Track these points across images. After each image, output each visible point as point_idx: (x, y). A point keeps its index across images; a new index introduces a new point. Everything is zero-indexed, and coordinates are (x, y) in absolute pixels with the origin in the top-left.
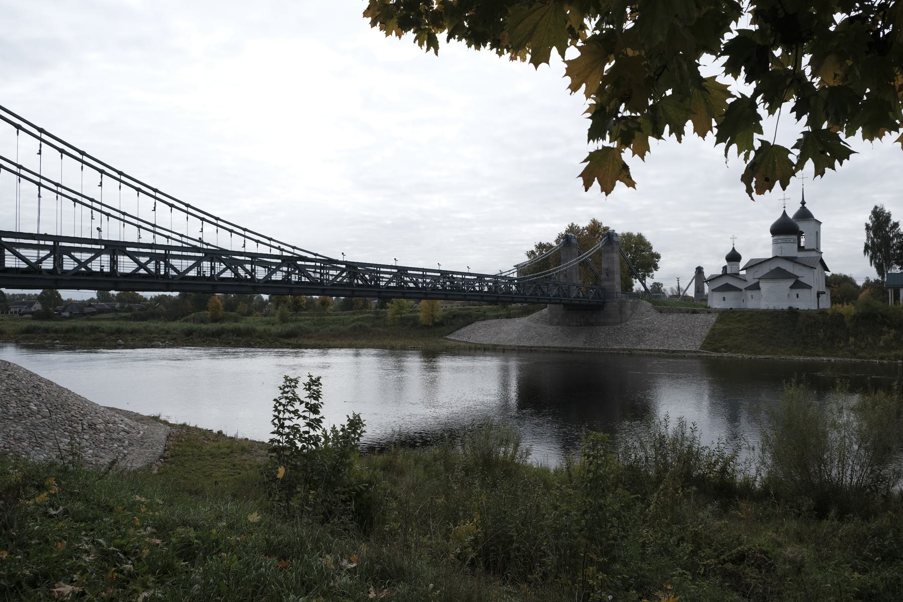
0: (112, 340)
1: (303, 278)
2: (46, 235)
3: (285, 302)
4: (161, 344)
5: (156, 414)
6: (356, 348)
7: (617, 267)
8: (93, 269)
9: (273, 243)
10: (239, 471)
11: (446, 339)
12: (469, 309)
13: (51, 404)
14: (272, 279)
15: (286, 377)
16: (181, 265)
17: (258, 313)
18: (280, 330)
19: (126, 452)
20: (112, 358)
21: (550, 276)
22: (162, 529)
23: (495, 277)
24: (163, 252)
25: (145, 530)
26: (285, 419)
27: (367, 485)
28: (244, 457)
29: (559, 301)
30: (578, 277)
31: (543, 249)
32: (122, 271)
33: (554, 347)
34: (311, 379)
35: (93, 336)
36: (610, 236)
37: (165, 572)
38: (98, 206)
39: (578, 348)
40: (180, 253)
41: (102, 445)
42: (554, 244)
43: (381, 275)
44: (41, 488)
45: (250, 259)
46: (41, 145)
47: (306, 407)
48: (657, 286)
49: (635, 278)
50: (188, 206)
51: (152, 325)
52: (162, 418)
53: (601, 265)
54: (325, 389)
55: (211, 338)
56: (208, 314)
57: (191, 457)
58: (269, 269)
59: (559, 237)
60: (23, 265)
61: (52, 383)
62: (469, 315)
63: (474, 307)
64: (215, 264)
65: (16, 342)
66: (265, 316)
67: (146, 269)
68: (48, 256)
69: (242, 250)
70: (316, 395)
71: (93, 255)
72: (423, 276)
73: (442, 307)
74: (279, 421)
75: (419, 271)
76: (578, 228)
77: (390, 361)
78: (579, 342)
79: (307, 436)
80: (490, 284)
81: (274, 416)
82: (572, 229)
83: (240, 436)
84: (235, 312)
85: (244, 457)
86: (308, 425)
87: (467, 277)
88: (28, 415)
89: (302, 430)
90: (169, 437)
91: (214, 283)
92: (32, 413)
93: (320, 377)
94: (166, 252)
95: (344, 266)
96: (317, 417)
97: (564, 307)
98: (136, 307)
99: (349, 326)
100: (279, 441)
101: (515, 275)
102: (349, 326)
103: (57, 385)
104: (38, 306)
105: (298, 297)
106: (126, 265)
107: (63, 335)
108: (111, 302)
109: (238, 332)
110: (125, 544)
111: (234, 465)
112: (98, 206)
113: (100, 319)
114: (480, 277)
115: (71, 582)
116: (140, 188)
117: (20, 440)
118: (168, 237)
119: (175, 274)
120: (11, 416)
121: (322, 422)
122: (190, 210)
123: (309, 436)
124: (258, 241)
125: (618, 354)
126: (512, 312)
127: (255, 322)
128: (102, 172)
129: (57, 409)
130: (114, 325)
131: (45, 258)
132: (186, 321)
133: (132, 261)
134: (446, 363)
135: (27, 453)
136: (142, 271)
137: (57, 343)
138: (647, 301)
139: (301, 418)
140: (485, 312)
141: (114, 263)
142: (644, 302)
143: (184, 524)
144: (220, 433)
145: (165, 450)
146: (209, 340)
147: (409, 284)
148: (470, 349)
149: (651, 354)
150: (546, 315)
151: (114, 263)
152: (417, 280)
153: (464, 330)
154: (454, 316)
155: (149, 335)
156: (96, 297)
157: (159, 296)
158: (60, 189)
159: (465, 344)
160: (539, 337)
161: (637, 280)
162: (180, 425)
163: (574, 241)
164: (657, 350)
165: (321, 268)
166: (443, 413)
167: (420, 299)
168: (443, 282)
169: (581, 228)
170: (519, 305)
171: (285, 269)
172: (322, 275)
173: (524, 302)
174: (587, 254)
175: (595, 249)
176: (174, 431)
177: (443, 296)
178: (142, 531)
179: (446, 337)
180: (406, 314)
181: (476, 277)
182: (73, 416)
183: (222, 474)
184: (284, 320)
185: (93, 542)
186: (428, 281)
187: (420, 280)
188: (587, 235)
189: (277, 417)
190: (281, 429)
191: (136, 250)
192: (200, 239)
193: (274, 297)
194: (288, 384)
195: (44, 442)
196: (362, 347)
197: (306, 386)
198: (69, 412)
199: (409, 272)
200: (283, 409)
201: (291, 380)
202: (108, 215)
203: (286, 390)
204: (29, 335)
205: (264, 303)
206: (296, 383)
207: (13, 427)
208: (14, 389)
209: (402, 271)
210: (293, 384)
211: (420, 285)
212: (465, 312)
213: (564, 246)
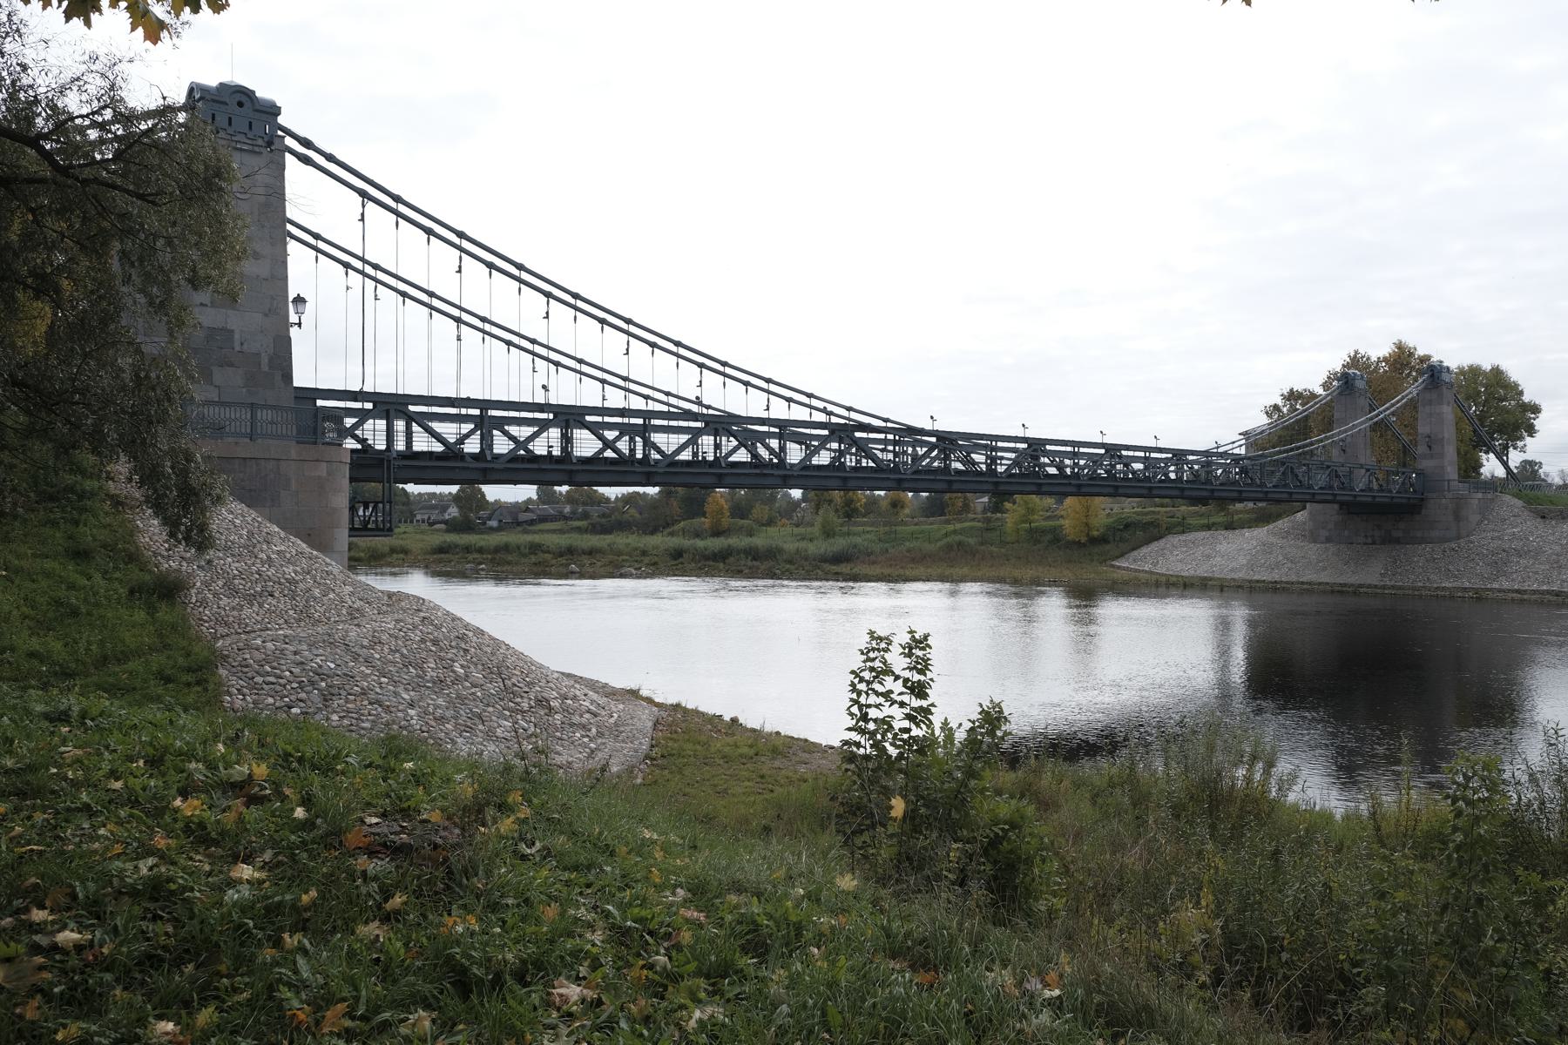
0: (562, 565)
1: (864, 461)
2: (468, 399)
3: (830, 501)
4: (634, 572)
5: (634, 686)
6: (952, 582)
7: (1449, 433)
8: (536, 452)
9: (815, 402)
10: (770, 786)
11: (1113, 566)
12: (1154, 512)
13: (483, 665)
14: (813, 462)
15: (871, 633)
16: (667, 442)
17: (784, 520)
18: (823, 550)
19: (592, 745)
20: (560, 594)
21: (1311, 451)
22: (699, 892)
23: (1207, 453)
24: (640, 421)
25: (674, 894)
26: (869, 706)
27: (1007, 827)
28: (777, 764)
29: (1330, 498)
30: (1368, 452)
31: (1296, 400)
32: (579, 454)
33: (1320, 584)
34: (913, 636)
35: (533, 559)
36: (1434, 374)
37: (717, 974)
38: (543, 351)
39: (1369, 586)
40: (665, 423)
41: (558, 734)
42: (1320, 391)
43: (999, 454)
44: (504, 808)
45: (777, 430)
46: (460, 257)
47: (905, 686)
48: (1530, 467)
49: (1487, 452)
50: (678, 344)
51: (621, 540)
52: (644, 693)
53: (1415, 428)
54: (937, 655)
55: (711, 563)
56: (706, 522)
57: (692, 759)
58: (807, 447)
59: (1329, 378)
60: (438, 448)
61: (482, 633)
62: (1153, 524)
63: (1164, 509)
64: (721, 440)
65: (426, 567)
66: (797, 526)
67: (615, 450)
68: (472, 432)
69: (765, 415)
70: (922, 666)
71: (536, 429)
72: (1074, 455)
73: (1105, 510)
74: (860, 709)
75: (1067, 445)
76: (1368, 359)
77: (1012, 607)
78: (1371, 573)
79: (906, 736)
80: (1196, 467)
81: (852, 700)
82: (1355, 361)
83: (768, 728)
84: (747, 519)
85: (777, 764)
86: (909, 717)
87: (1153, 455)
88: (451, 681)
89: (897, 725)
90: (656, 723)
91: (720, 471)
92: (457, 680)
93: (929, 635)
94: (645, 421)
95: (933, 439)
96: (924, 703)
97: (1341, 509)
98: (594, 511)
99: (939, 544)
100: (858, 745)
101: (1243, 451)
102: (939, 544)
103: (490, 636)
104: (453, 512)
105: (851, 493)
106: (585, 444)
107: (489, 556)
108: (558, 503)
109: (754, 554)
110: (649, 917)
111: (762, 777)
112: (543, 351)
113: (541, 531)
114: (1179, 456)
115: (578, 979)
116: (606, 318)
117: (441, 720)
118: (647, 397)
119: (658, 457)
120: (428, 682)
121: (932, 714)
122: (682, 351)
123: (910, 737)
124: (789, 400)
125: (1452, 597)
126: (1236, 517)
127: (779, 536)
128: (548, 295)
129: (492, 673)
130: (563, 541)
131: (467, 436)
132: (672, 534)
133: (593, 437)
134: (1112, 610)
135: (454, 742)
136: (609, 454)
137: (482, 569)
138: (1513, 495)
139: (896, 706)
140: (1184, 519)
141: (567, 440)
142: (1507, 498)
143: (739, 888)
144: (734, 720)
145: (652, 746)
146: (709, 566)
147: (1047, 469)
148: (1157, 584)
149: (1521, 599)
150: (1305, 523)
151: (567, 440)
152: (1062, 462)
153: (1144, 550)
154: (1127, 526)
155: (616, 557)
156: (535, 497)
157: (629, 494)
158: (487, 327)
159: (1147, 576)
160: (1289, 565)
161: (1491, 456)
162: (672, 705)
163: (1360, 384)
164: (1534, 592)
165: (895, 443)
166: (1107, 699)
167: (1066, 495)
168: (1110, 465)
169: (1374, 359)
170: (1250, 505)
171: (835, 445)
172: (896, 454)
173: (1260, 500)
174: (1388, 409)
175: (1403, 398)
176: (664, 714)
177: (1111, 490)
178: (668, 894)
179: (1113, 563)
180: (1039, 522)
181: (1170, 455)
182: (514, 685)
183: (744, 790)
184: (828, 533)
185: (595, 908)
186: (1082, 462)
187: (1067, 462)
188: (1385, 372)
189: (856, 702)
190: (861, 723)
191: (599, 419)
192: (697, 398)
193: (812, 494)
194: (874, 645)
195: (475, 724)
196: (963, 579)
197: (904, 649)
198: (509, 679)
199: (1048, 447)
200: (865, 689)
201: (881, 639)
202: (557, 364)
203: (872, 655)
204: (443, 556)
205: (795, 504)
206: (888, 644)
207: (432, 699)
208: (431, 640)
209: (1036, 447)
210: (883, 645)
211: (1068, 471)
212: (1148, 518)
213: (1340, 394)
